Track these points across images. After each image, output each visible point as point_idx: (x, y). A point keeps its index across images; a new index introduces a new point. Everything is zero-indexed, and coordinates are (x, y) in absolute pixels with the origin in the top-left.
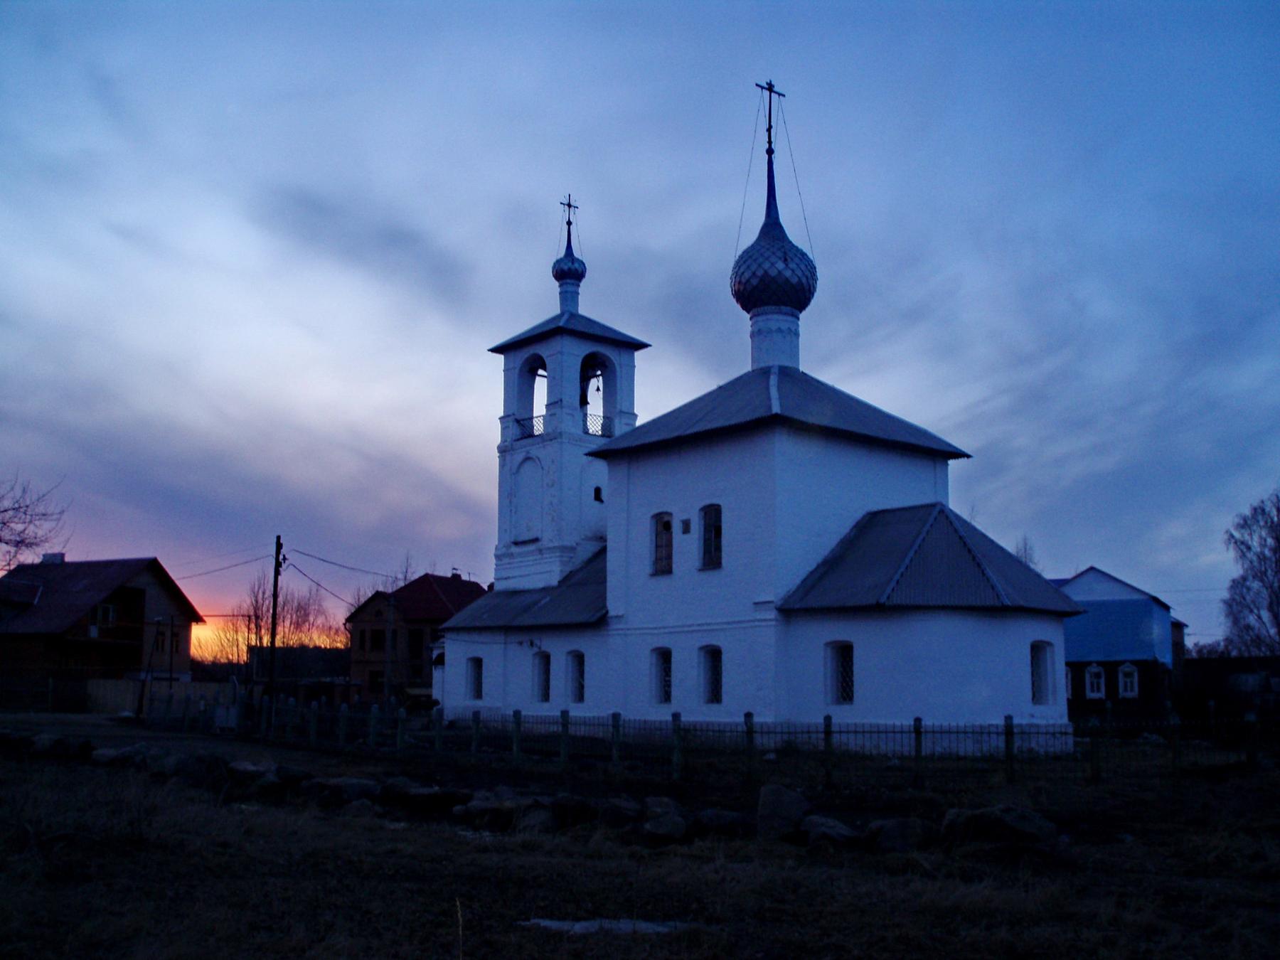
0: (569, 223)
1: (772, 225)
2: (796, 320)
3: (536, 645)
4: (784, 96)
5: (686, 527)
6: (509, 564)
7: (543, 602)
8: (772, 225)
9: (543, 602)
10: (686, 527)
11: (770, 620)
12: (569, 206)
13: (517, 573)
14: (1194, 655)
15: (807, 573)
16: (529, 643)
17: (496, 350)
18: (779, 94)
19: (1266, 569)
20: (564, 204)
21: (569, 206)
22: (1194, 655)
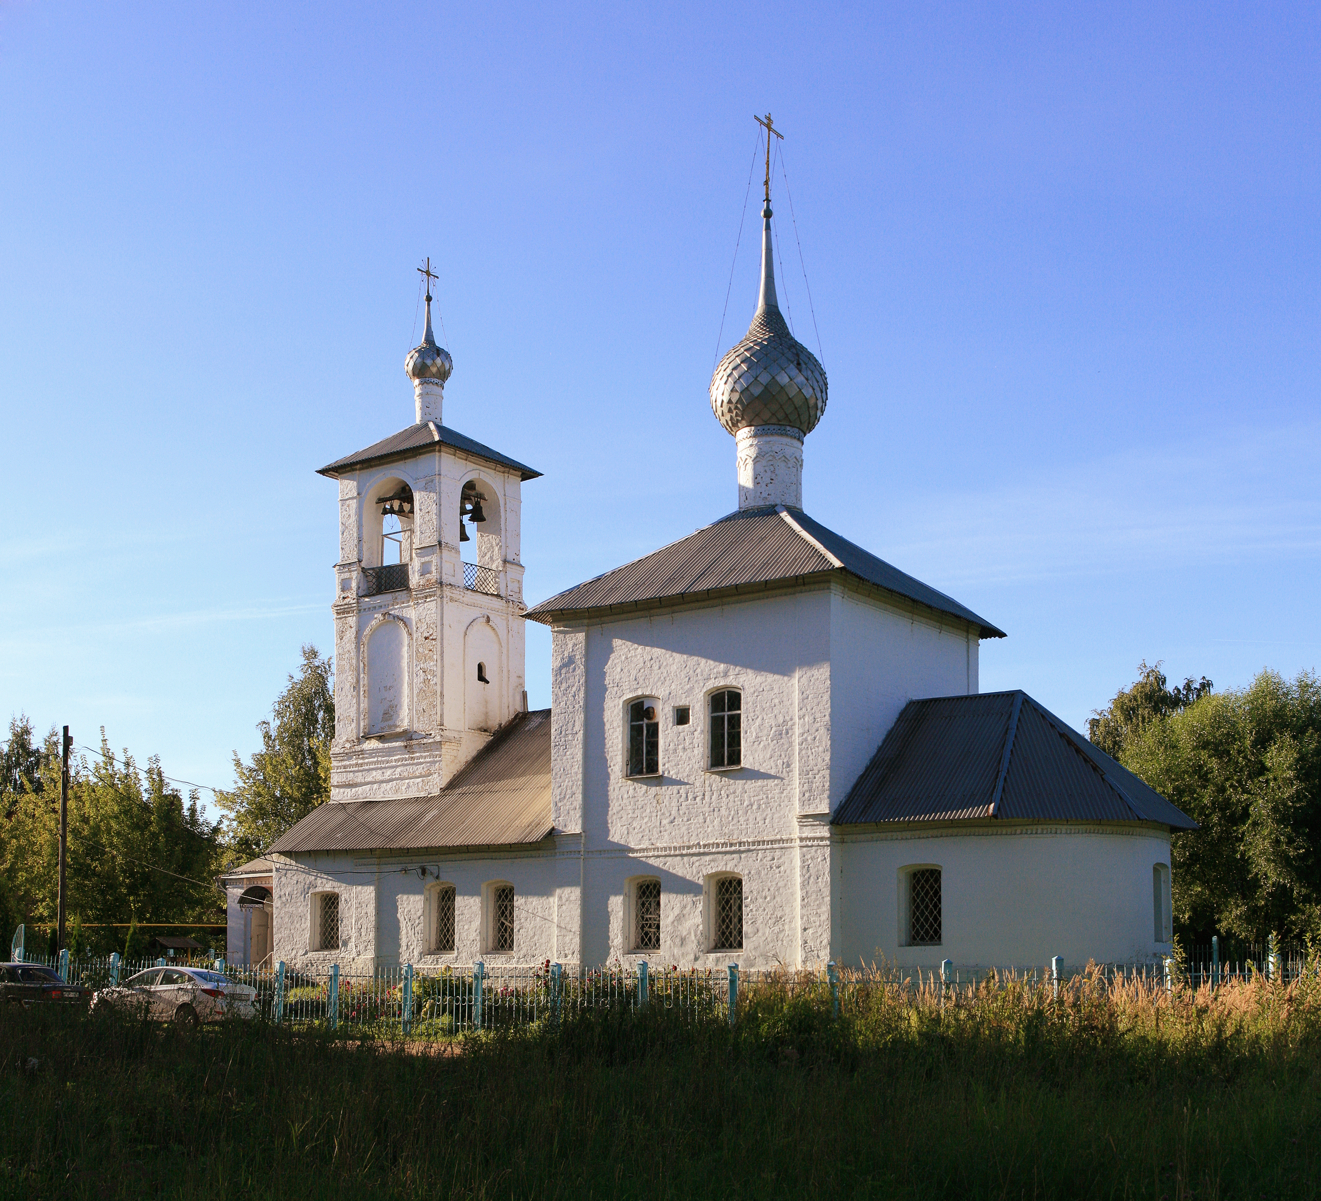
0: (429, 299)
1: (429, 339)
2: (799, 444)
3: (431, 873)
4: (782, 137)
5: (682, 716)
6: (357, 764)
7: (429, 817)
8: (429, 339)
9: (429, 817)
10: (682, 716)
11: (822, 839)
12: (428, 273)
13: (377, 775)
14: (721, 1010)
15: (857, 777)
16: (420, 871)
17: (334, 471)
18: (779, 135)
19: (249, 983)
20: (422, 271)
21: (428, 273)
22: (721, 1010)
